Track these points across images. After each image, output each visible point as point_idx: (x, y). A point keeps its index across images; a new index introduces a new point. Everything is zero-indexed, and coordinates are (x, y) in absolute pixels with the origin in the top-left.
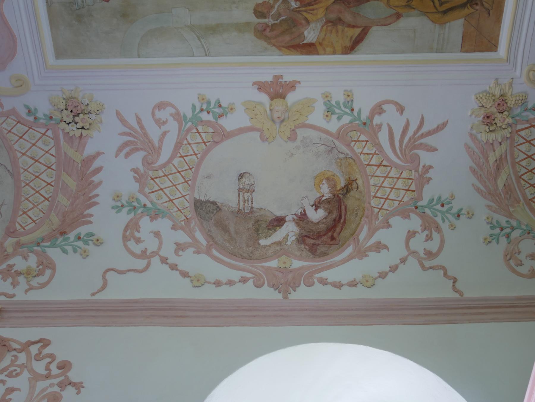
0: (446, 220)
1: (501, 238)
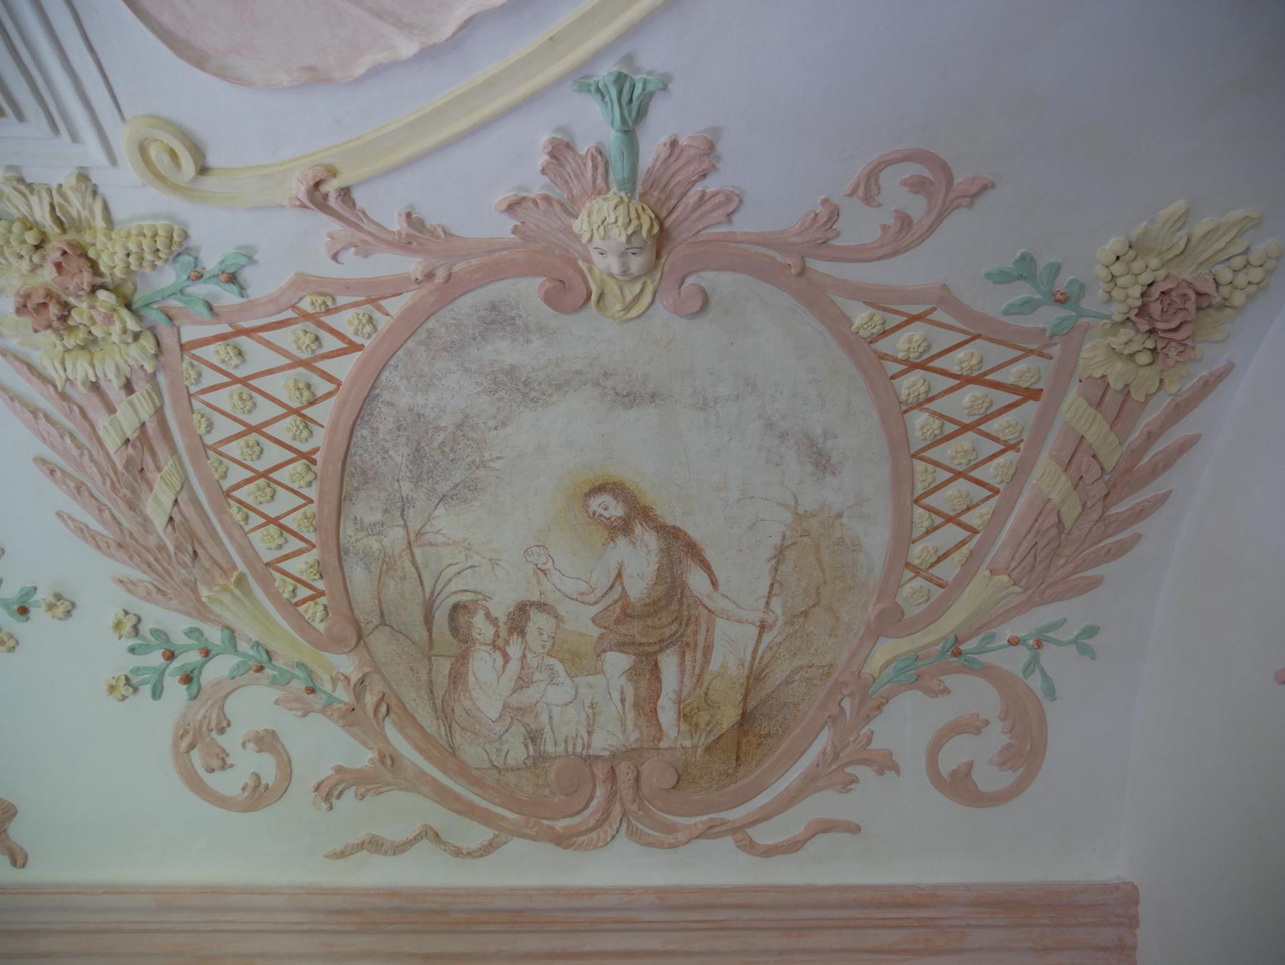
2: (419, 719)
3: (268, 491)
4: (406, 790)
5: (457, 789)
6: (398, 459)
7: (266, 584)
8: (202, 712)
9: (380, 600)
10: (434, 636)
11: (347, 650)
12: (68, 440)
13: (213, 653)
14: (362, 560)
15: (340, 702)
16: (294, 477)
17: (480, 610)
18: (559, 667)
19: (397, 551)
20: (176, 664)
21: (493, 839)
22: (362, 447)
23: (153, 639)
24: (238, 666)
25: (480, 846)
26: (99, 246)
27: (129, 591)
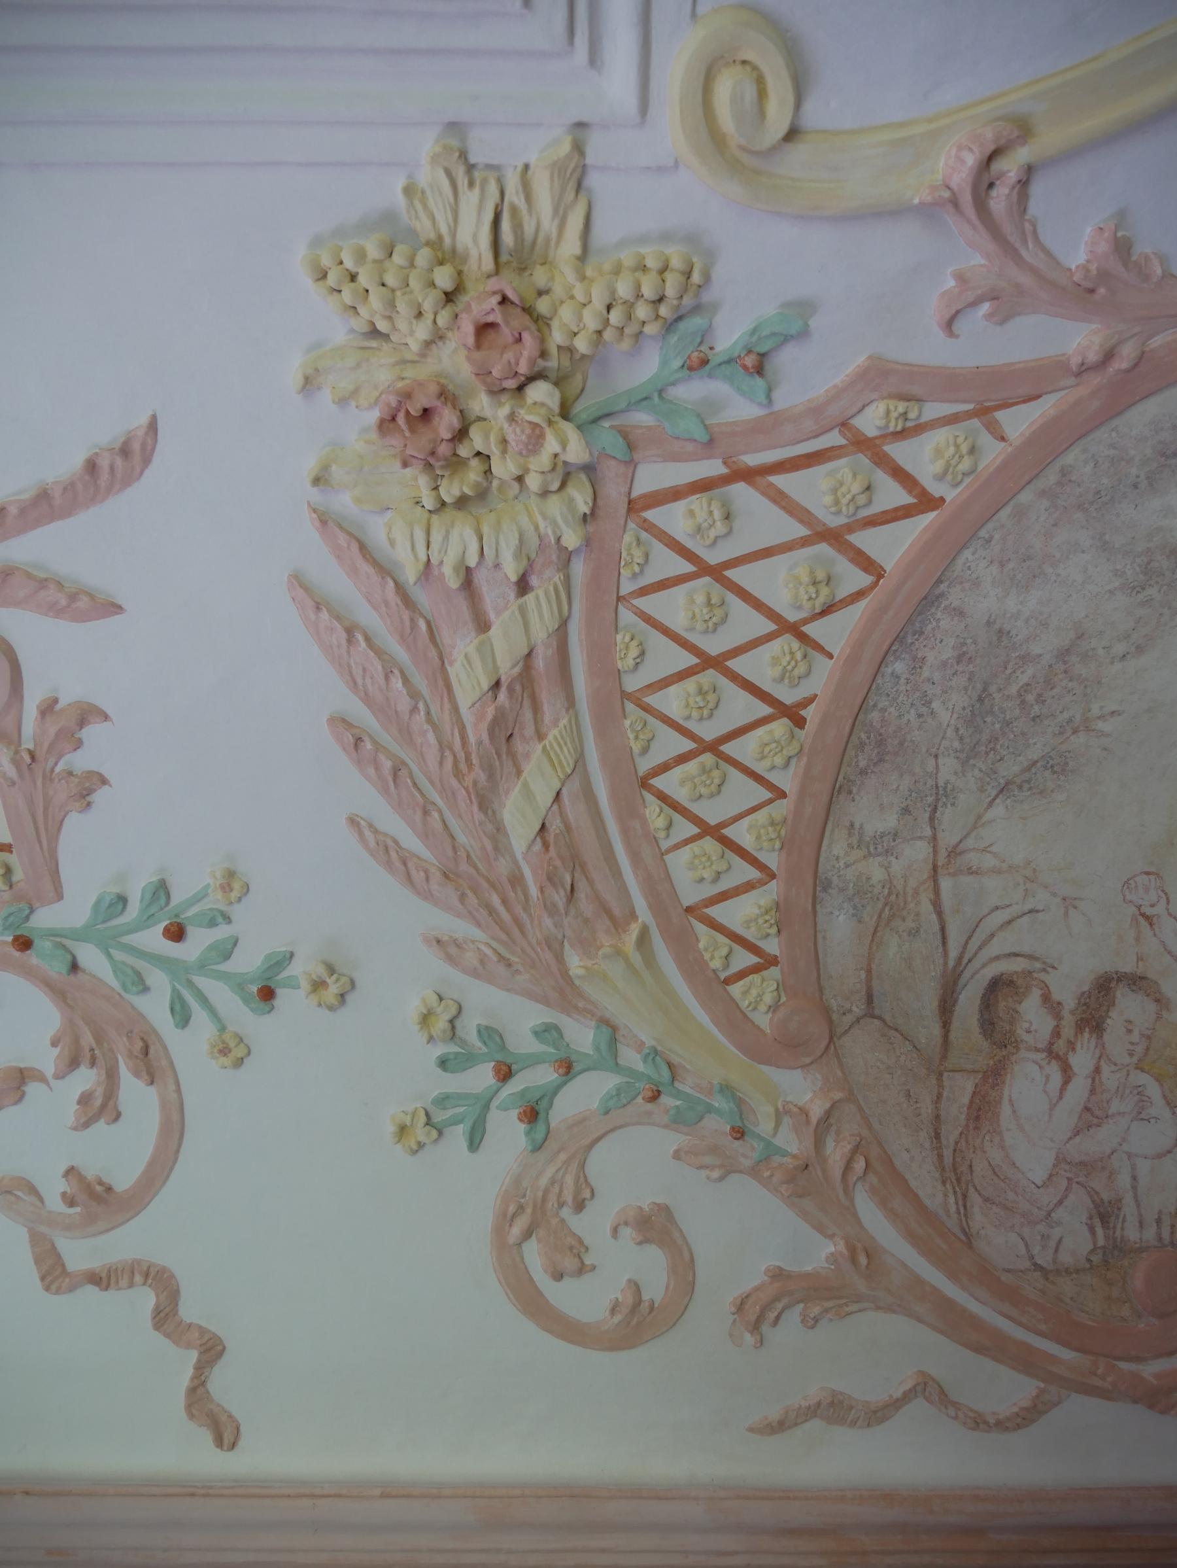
0: (199, 1015)
1: (495, 1118)
2: (913, 1183)
3: (716, 774)
4: (889, 1309)
5: (974, 1307)
6: (944, 716)
7: (682, 945)
8: (550, 1172)
9: (869, 972)
10: (953, 1035)
11: (808, 1060)
12: (396, 683)
13: (577, 1067)
14: (850, 900)
15: (785, 1154)
16: (767, 750)
17: (1034, 989)
18: (1153, 1090)
19: (912, 883)
20: (515, 1086)
21: (1038, 1396)
22: (888, 695)
23: (479, 1044)
24: (619, 1091)
25: (1015, 1409)
26: (558, 290)
27: (450, 959)
